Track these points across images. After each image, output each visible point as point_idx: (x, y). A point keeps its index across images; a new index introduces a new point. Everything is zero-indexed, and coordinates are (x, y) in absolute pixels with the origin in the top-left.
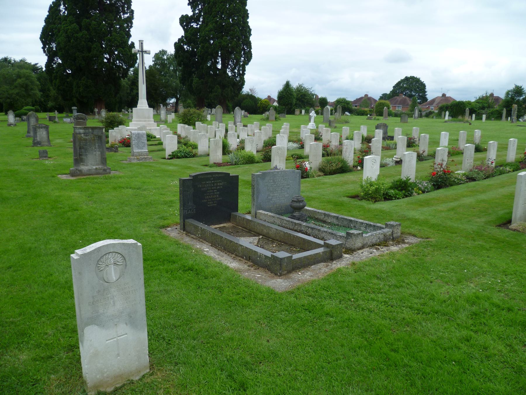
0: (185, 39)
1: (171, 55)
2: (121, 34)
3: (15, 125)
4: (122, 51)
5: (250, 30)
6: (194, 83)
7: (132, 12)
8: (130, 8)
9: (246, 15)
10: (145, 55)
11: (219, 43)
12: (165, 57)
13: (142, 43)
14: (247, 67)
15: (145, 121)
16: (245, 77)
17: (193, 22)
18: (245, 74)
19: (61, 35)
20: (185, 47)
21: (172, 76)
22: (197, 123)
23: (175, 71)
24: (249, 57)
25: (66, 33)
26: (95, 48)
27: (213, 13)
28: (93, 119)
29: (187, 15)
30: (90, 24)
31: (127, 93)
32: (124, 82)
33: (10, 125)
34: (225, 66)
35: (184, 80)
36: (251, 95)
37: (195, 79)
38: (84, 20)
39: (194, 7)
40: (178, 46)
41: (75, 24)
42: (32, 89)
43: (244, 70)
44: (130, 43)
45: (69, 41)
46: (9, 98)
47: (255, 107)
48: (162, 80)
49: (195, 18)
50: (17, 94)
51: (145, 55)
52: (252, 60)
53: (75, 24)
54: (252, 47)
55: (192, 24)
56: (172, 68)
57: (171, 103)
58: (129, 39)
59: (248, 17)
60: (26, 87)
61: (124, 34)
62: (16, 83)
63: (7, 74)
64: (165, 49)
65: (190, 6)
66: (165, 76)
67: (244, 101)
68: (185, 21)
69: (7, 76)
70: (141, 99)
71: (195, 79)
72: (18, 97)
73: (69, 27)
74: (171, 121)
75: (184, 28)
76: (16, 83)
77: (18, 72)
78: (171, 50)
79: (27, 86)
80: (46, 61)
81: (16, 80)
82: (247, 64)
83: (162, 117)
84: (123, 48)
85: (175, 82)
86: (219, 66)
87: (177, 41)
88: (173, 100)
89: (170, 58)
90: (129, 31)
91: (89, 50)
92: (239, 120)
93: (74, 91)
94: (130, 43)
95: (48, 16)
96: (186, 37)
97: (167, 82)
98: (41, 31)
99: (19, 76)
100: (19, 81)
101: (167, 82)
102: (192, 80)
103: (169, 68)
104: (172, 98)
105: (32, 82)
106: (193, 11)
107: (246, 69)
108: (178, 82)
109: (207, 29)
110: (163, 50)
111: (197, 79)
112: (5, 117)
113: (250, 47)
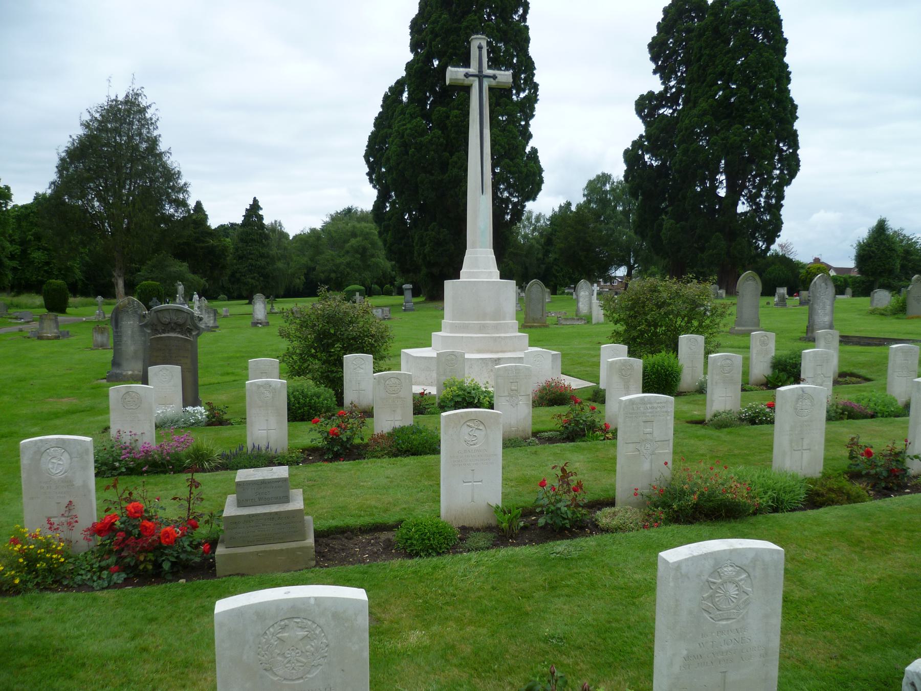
1: (620, 183)
2: (510, 132)
3: (267, 324)
4: (509, 166)
5: (795, 107)
6: (664, 231)
7: (535, 87)
8: (532, 79)
9: (784, 76)
11: (723, 139)
12: (608, 187)
14: (788, 190)
15: (482, 328)
16: (783, 212)
17: (663, 107)
18: (782, 206)
20: (647, 157)
22: (683, 338)
23: (625, 213)
24: (792, 166)
25: (403, 137)
26: (456, 163)
27: (708, 79)
29: (651, 94)
30: (448, 117)
31: (538, 260)
33: (255, 324)
34: (734, 192)
35: (641, 228)
36: (784, 256)
37: (667, 222)
39: (665, 79)
40: (632, 157)
42: (373, 256)
43: (781, 197)
44: (528, 149)
45: (407, 153)
46: (335, 272)
47: (791, 278)
48: (601, 231)
50: (348, 264)
52: (799, 174)
53: (419, 119)
55: (661, 112)
56: (620, 208)
57: (620, 277)
58: (527, 143)
59: (789, 81)
60: (363, 252)
61: (515, 130)
63: (335, 232)
65: (658, 75)
66: (608, 223)
67: (769, 269)
69: (334, 234)
70: (474, 247)
71: (667, 222)
73: (409, 126)
75: (645, 122)
76: (347, 246)
77: (354, 227)
78: (618, 171)
79: (365, 249)
80: (375, 199)
82: (788, 183)
83: (581, 305)
84: (512, 160)
85: (626, 235)
86: (722, 192)
87: (629, 145)
88: (622, 272)
89: (617, 187)
90: (527, 125)
92: (827, 319)
93: (416, 254)
94: (528, 149)
96: (648, 136)
97: (611, 235)
99: (354, 235)
100: (353, 241)
101: (611, 235)
102: (661, 225)
103: (615, 207)
104: (620, 266)
105: (373, 244)
106: (663, 83)
107: (786, 193)
108: (632, 233)
109: (695, 111)
110: (604, 174)
111: (673, 221)
112: (247, 309)
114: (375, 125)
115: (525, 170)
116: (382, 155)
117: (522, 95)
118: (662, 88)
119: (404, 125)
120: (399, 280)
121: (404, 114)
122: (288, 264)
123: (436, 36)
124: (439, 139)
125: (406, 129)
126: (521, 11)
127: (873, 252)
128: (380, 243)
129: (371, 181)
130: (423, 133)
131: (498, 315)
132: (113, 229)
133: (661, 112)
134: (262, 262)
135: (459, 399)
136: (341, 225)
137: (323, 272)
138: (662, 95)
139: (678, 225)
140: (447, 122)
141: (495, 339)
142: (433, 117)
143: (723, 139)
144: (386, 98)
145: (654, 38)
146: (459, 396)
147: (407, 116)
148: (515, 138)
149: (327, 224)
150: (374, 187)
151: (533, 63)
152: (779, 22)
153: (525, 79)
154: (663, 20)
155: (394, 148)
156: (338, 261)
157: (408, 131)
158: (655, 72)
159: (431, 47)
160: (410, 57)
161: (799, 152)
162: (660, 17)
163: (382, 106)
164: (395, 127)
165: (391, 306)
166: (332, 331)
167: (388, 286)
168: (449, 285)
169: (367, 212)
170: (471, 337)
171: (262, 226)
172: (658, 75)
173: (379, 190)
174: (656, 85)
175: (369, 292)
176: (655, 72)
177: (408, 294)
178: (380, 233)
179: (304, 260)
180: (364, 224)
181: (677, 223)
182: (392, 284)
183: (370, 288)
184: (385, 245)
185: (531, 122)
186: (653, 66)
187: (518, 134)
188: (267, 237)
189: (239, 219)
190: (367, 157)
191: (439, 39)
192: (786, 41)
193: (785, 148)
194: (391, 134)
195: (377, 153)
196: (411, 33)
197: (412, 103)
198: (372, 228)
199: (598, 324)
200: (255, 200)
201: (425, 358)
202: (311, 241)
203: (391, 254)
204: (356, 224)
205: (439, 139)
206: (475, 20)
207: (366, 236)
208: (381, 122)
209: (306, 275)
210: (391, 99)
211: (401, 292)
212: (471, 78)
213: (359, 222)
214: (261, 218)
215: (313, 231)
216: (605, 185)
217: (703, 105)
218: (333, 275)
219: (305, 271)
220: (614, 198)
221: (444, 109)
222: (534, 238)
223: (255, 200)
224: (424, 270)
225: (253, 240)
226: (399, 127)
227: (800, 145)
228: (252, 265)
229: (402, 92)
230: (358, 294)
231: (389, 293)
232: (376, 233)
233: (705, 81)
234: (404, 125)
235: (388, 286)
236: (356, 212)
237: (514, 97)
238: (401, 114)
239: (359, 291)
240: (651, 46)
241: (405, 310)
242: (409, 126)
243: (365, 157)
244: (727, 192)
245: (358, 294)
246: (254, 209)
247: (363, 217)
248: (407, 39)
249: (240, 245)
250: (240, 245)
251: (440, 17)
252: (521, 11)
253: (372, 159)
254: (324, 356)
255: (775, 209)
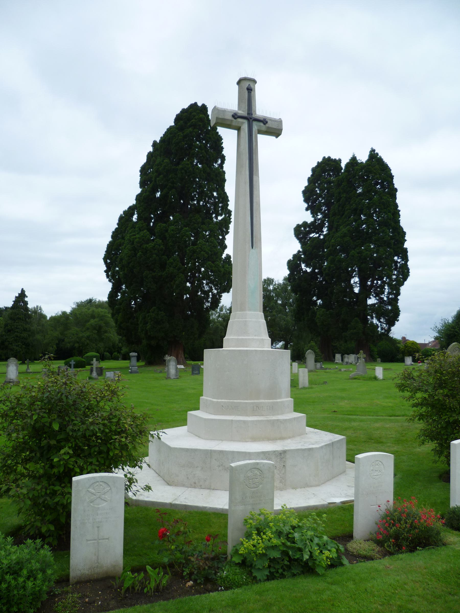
0: (304, 254)
1: (279, 285)
5: (404, 233)
10: (264, 142)
11: (358, 253)
12: (271, 287)
13: (250, 90)
15: (256, 409)
19: (125, 247)
20: (303, 266)
21: (280, 312)
24: (404, 273)
28: (161, 372)
30: (167, 231)
32: (214, 316)
38: (159, 224)
39: (314, 214)
40: (293, 265)
41: (145, 231)
42: (106, 332)
44: (224, 256)
46: (78, 342)
47: (394, 352)
49: (315, 227)
50: (88, 338)
51: (264, 142)
53: (145, 231)
54: (409, 258)
58: (224, 251)
60: (99, 329)
61: (215, 241)
62: (88, 325)
63: (80, 314)
64: (271, 277)
65: (309, 212)
66: (271, 312)
68: (301, 232)
72: (88, 341)
73: (138, 236)
74: (307, 384)
75: (300, 242)
76: (88, 325)
77: (93, 311)
79: (100, 327)
81: (88, 321)
84: (213, 262)
87: (291, 257)
90: (224, 239)
91: (163, 266)
93: (139, 330)
94: (224, 256)
95: (116, 229)
98: (105, 249)
99: (93, 317)
100: (92, 321)
103: (277, 301)
105: (107, 324)
106: (313, 217)
108: (289, 318)
109: (338, 234)
113: (405, 257)
114: (112, 237)
115: (222, 270)
116: (117, 258)
117: (220, 218)
118: (312, 219)
119: (134, 235)
120: (124, 350)
121: (135, 228)
122: (45, 336)
123: (160, 174)
124: (160, 245)
125: (136, 238)
126: (219, 162)
127: (457, 332)
128: (113, 323)
129: (108, 276)
130: (149, 241)
131: (273, 392)
132: (6, 332)
133: (311, 236)
134: (25, 335)
135: (276, 554)
136: (84, 310)
137: (69, 343)
138: (313, 223)
139: (328, 312)
140: (166, 234)
141: (273, 423)
142: (156, 231)
143: (358, 253)
144: (121, 218)
145: (306, 187)
146: (274, 547)
147: (136, 229)
148: (216, 247)
149: (74, 309)
150: (110, 281)
151: (227, 197)
152: (392, 177)
153: (222, 207)
154: (312, 175)
155: (126, 251)
156: (81, 335)
157: (137, 240)
158: (307, 209)
159: (155, 181)
160: (139, 191)
161: (408, 263)
162: (309, 174)
163: (118, 224)
164: (127, 237)
165: (120, 369)
166: (56, 427)
167: (116, 353)
168: (208, 353)
169: (103, 302)
170: (244, 422)
171: (27, 309)
172: (309, 212)
173: (113, 283)
174: (309, 218)
175: (102, 358)
176: (307, 209)
177: (134, 360)
178: (113, 315)
179: (56, 334)
180: (100, 310)
181: (327, 311)
182: (119, 352)
183: (103, 355)
184: (116, 323)
185: (227, 237)
186: (306, 205)
187: (217, 244)
188: (30, 317)
189: (9, 304)
190: (105, 259)
191: (162, 176)
192: (396, 190)
193: (399, 260)
194: (124, 243)
195: (113, 257)
196: (141, 175)
197: (140, 220)
198: (107, 313)
199: (304, 388)
200: (23, 291)
201: (187, 450)
202: (62, 320)
203: (121, 329)
204: (94, 309)
205: (160, 245)
206: (188, 164)
207: (102, 318)
208: (117, 235)
209: (57, 344)
210: (125, 219)
211: (126, 357)
212: (239, 120)
213: (97, 308)
214: (26, 303)
215: (64, 313)
216: (269, 286)
217: (344, 229)
218: (77, 345)
219: (57, 342)
220: (276, 295)
221: (164, 225)
222: (219, 322)
223: (23, 291)
224: (144, 342)
225: (19, 319)
226: (130, 237)
227: (409, 258)
228: (17, 336)
229: (133, 214)
230: (95, 359)
231: (116, 359)
232: (110, 315)
233: (343, 214)
234: (134, 235)
235: (116, 353)
236: (95, 302)
237: (215, 220)
238: (132, 228)
239: (95, 357)
240: (304, 192)
241: (131, 372)
242: (138, 236)
243: (104, 259)
244: (360, 290)
245: (95, 359)
246: (21, 297)
247: (100, 305)
248: (138, 179)
249: (10, 322)
250: (10, 322)
251: (163, 161)
252: (219, 162)
253: (109, 261)
254: (38, 468)
255: (394, 302)
